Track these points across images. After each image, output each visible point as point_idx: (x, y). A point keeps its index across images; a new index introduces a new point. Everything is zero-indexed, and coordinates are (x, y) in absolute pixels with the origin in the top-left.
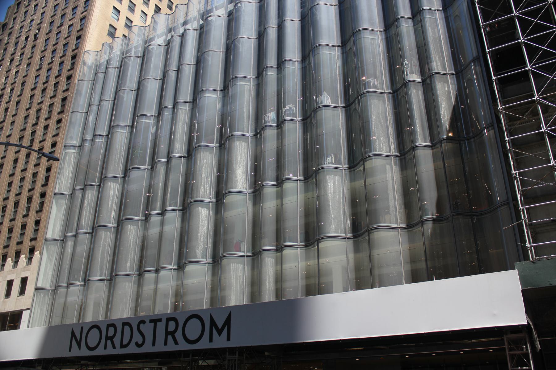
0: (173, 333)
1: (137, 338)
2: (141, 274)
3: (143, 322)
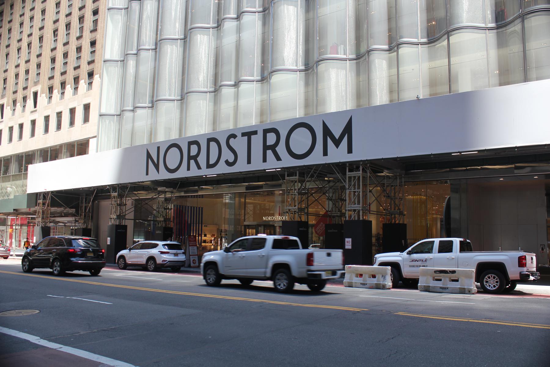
0: (273, 148)
1: (227, 155)
2: (217, 90)
3: (234, 136)
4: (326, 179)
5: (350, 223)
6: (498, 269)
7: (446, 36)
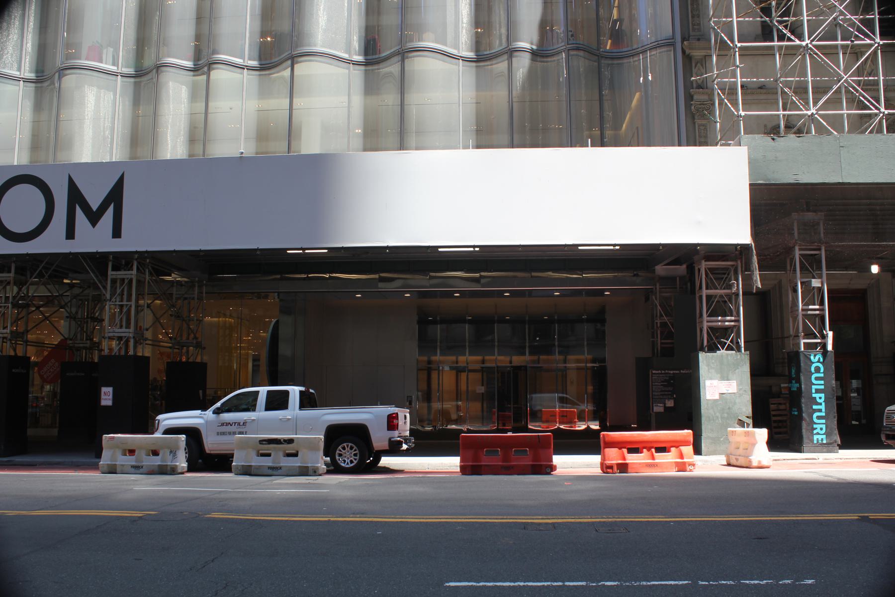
4: (65, 281)
5: (109, 360)
6: (357, 434)
7: (289, 62)
